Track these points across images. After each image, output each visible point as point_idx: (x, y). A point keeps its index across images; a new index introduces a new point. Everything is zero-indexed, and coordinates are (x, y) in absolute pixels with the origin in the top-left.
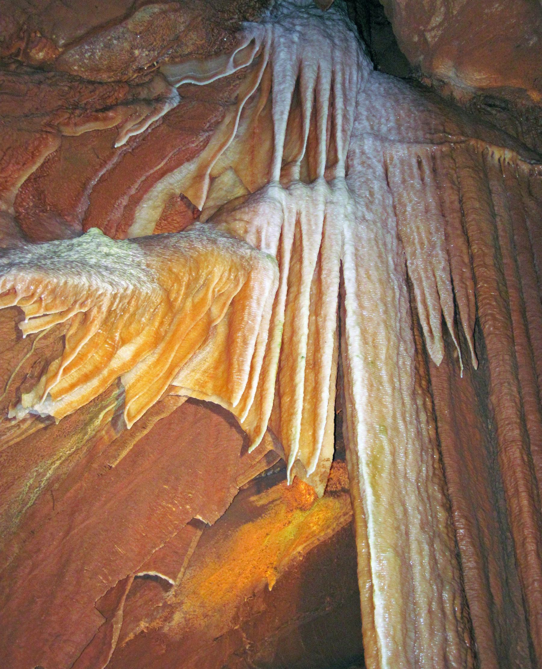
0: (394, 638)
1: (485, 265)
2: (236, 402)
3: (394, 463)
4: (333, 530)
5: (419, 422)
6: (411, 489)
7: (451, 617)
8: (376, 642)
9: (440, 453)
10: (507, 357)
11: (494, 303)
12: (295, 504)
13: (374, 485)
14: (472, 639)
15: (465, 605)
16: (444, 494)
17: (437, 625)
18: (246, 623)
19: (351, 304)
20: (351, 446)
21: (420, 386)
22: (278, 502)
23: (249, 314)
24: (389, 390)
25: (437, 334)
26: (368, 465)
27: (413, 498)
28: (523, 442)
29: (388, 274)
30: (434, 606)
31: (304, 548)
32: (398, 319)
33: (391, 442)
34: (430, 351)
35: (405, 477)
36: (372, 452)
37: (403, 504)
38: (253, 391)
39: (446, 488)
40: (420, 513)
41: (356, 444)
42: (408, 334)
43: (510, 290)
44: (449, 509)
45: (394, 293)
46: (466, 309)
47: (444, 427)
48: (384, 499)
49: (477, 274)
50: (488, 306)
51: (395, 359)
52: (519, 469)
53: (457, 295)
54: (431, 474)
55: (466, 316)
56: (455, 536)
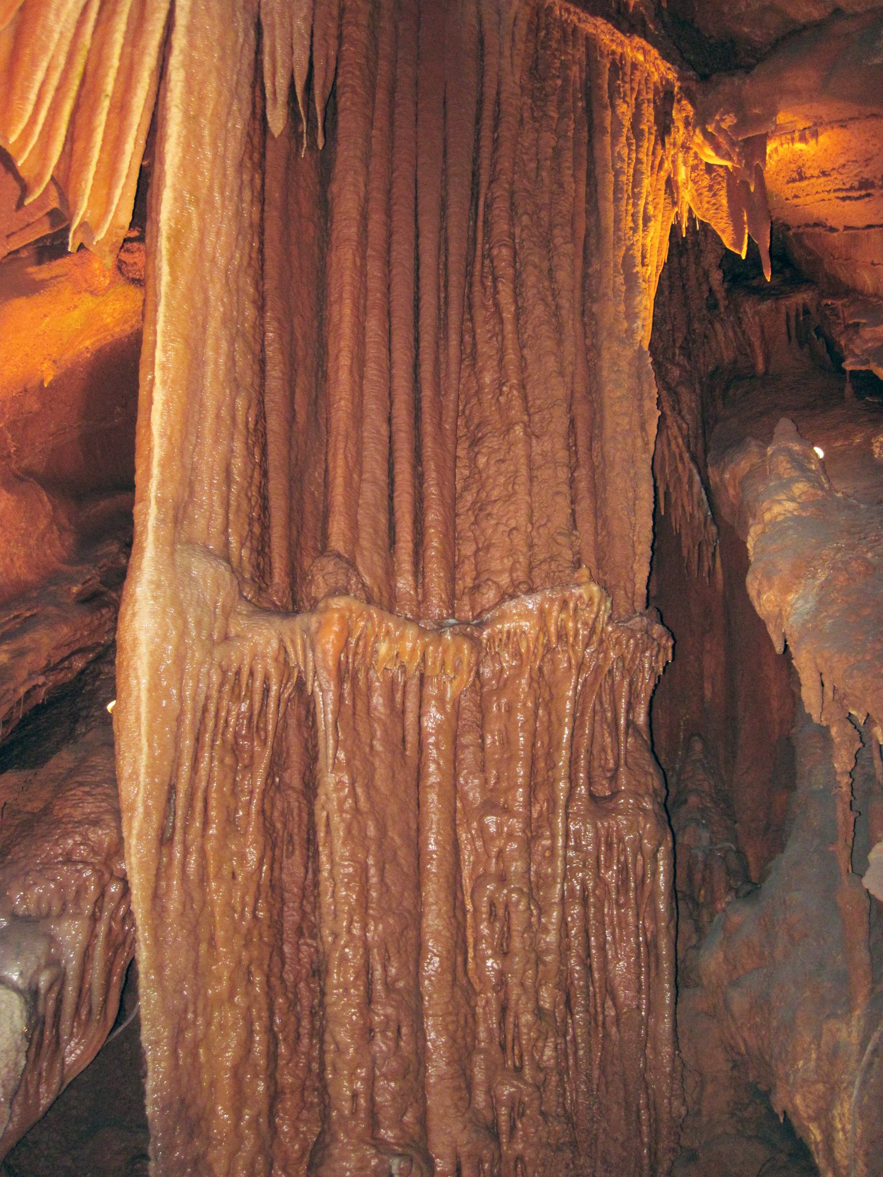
0: (170, 439)
1: (357, 25)
2: (13, 139)
3: (201, 241)
4: (132, 327)
5: (241, 200)
6: (218, 275)
7: (241, 427)
8: (149, 441)
9: (262, 243)
10: (360, 141)
11: (358, 73)
12: (84, 286)
13: (172, 264)
14: (264, 453)
15: (262, 417)
16: (257, 288)
17: (224, 433)
18: (14, 422)
19: (179, 40)
20: (153, 215)
21: (251, 158)
22: (62, 279)
23: (44, 27)
24: (209, 154)
25: (282, 98)
26: (169, 239)
27: (218, 286)
28: (359, 243)
29: (234, 11)
30: (224, 412)
31: (93, 344)
32: (236, 70)
33: (202, 218)
34: (269, 117)
35: (213, 261)
36: (176, 224)
37: (205, 291)
38: (38, 128)
39: (261, 283)
40: (223, 304)
41: (158, 213)
42: (246, 92)
43: (381, 62)
44: (261, 308)
45: (237, 36)
46: (323, 74)
47: (273, 214)
48: (182, 282)
49: (345, 33)
50: (349, 75)
51: (224, 118)
52: (348, 272)
53: (315, 54)
54: (245, 263)
55: (321, 83)
56: (263, 341)
